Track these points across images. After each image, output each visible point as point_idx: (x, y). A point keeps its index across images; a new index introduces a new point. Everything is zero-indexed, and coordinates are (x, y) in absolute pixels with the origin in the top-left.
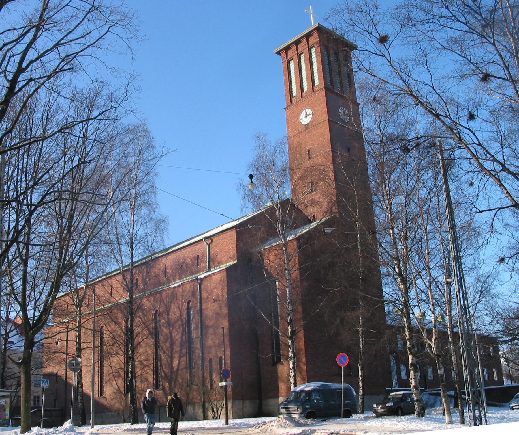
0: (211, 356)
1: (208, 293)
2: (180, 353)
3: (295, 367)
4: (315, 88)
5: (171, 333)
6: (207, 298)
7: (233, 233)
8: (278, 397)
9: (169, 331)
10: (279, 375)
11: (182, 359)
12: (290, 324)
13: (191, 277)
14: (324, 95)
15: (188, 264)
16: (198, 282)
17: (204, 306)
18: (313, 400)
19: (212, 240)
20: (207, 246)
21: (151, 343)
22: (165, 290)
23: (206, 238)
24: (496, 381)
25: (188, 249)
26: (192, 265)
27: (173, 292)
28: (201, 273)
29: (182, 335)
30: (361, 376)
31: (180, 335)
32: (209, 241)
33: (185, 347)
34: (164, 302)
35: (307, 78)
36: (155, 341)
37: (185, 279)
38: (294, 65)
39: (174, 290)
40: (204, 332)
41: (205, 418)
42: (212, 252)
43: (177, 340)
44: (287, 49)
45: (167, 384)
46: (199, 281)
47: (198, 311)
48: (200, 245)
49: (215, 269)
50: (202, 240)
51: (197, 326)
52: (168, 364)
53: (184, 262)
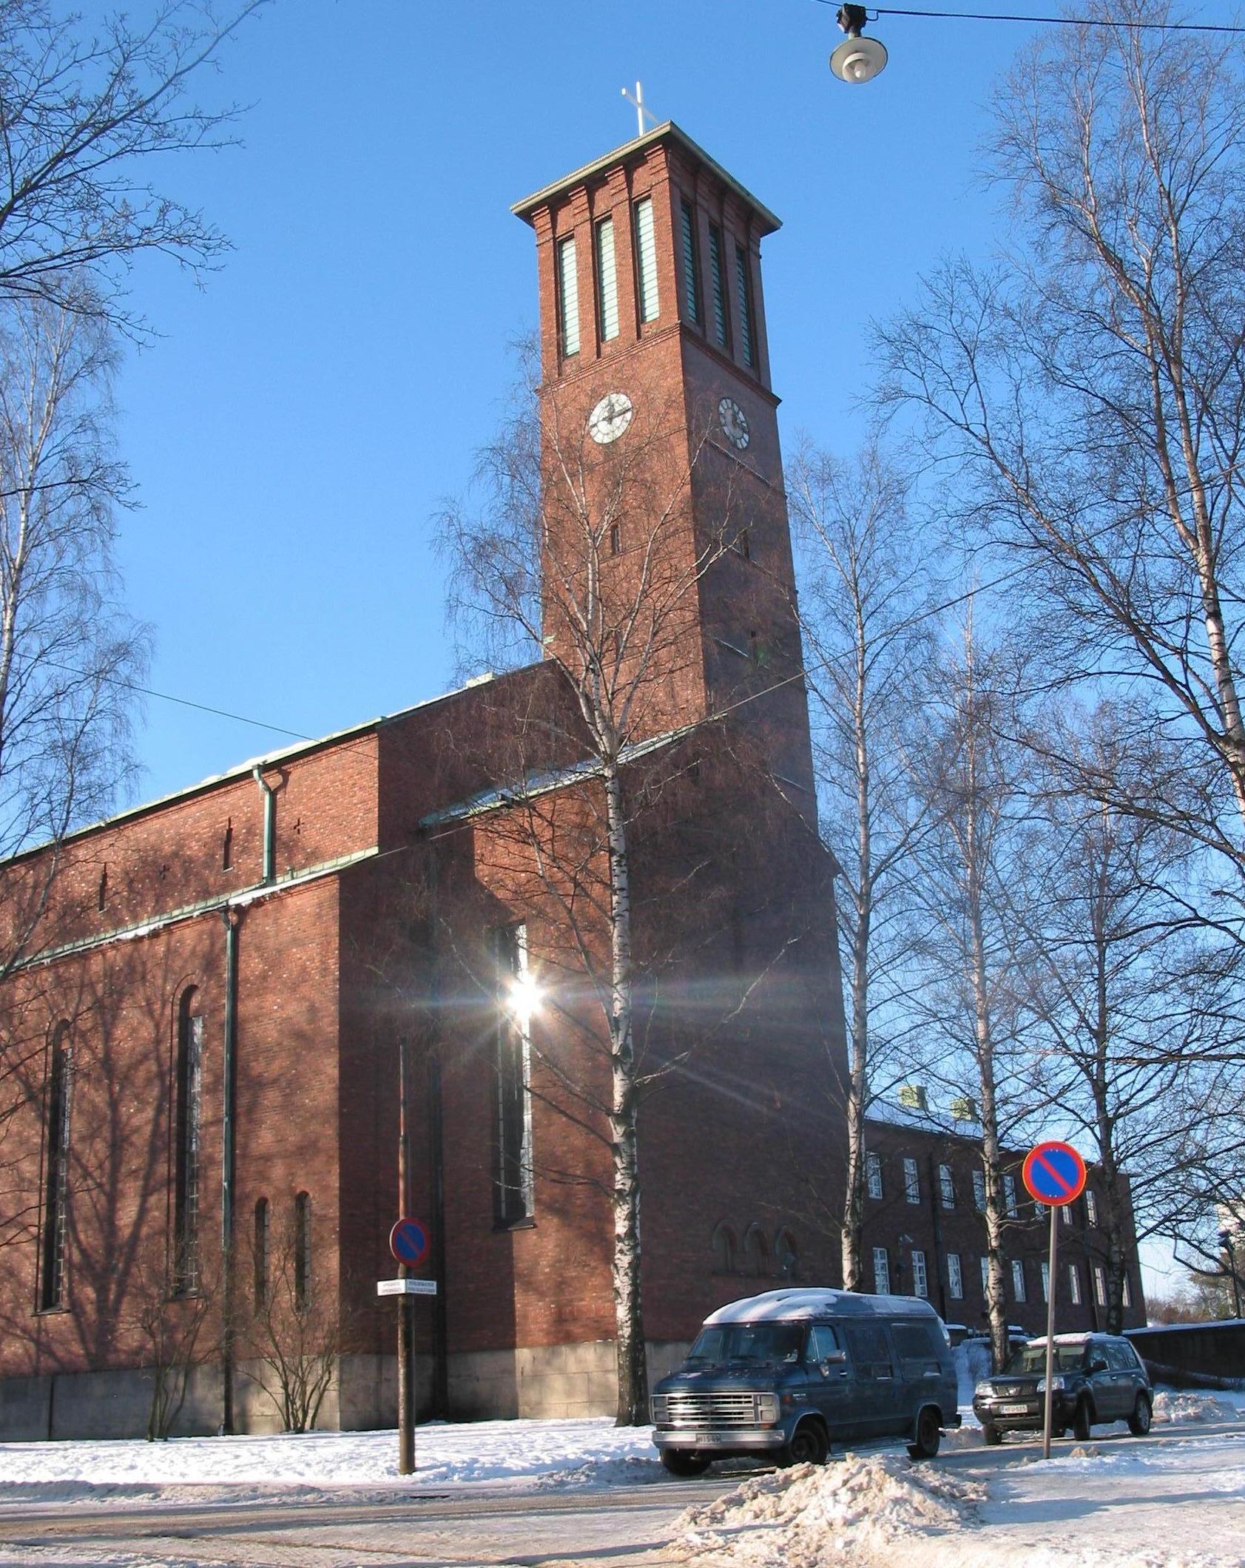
0: (267, 1191)
1: (265, 961)
2: (147, 1178)
3: (638, 1231)
4: (644, 328)
5: (114, 1104)
6: (264, 977)
7: (369, 748)
8: (512, 1346)
9: (107, 1097)
10: (521, 1266)
11: (153, 1200)
12: (622, 1063)
13: (203, 905)
14: (679, 349)
15: (191, 860)
16: (227, 921)
17: (246, 1008)
18: (817, 1367)
19: (286, 775)
20: (267, 797)
21: (37, 1140)
22: (100, 950)
23: (265, 768)
24: (1075, 1306)
25: (194, 809)
26: (207, 865)
27: (131, 956)
28: (240, 892)
29: (159, 1110)
30: (852, 1274)
31: (150, 1113)
32: (274, 780)
33: (164, 1156)
34: (94, 992)
35: (621, 296)
36: (51, 1134)
37: (176, 913)
38: (579, 253)
39: (136, 949)
40: (243, 1101)
41: (235, 1424)
42: (285, 818)
43: (137, 1130)
44: (557, 202)
45: (90, 1292)
46: (233, 918)
47: (222, 1025)
48: (239, 793)
49: (293, 878)
50: (248, 775)
51: (217, 1079)
52: (98, 1216)
53: (175, 855)
